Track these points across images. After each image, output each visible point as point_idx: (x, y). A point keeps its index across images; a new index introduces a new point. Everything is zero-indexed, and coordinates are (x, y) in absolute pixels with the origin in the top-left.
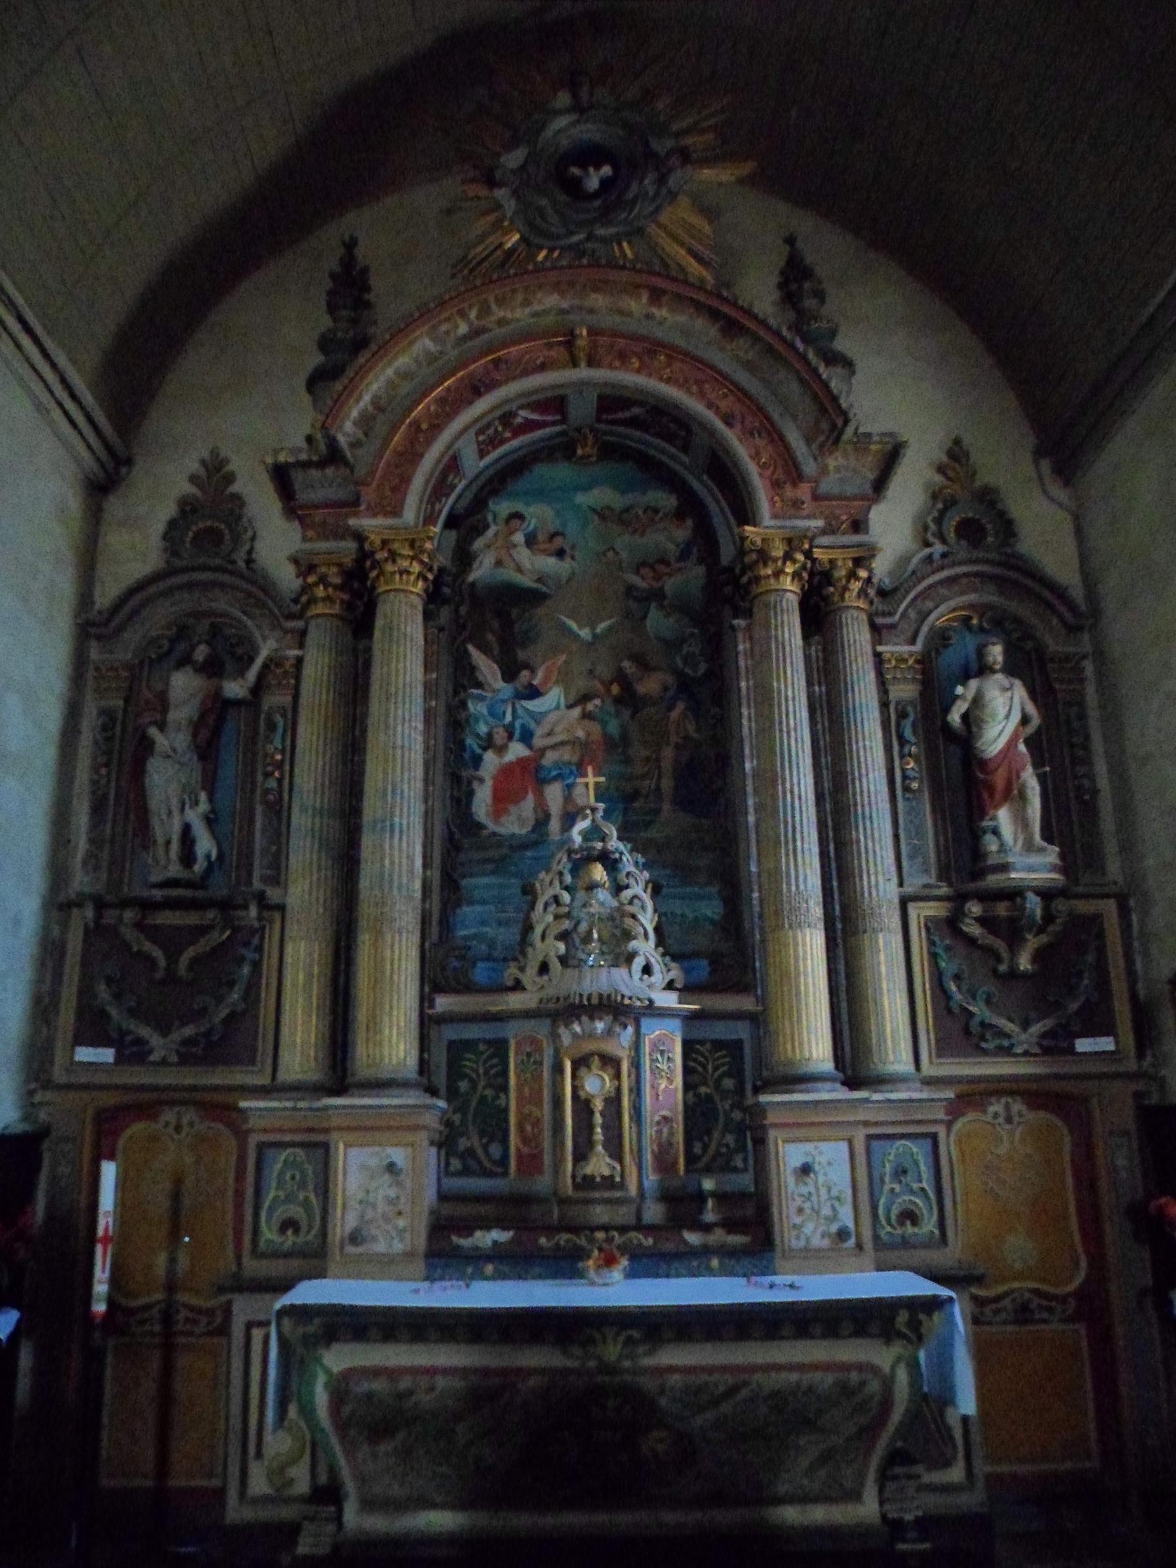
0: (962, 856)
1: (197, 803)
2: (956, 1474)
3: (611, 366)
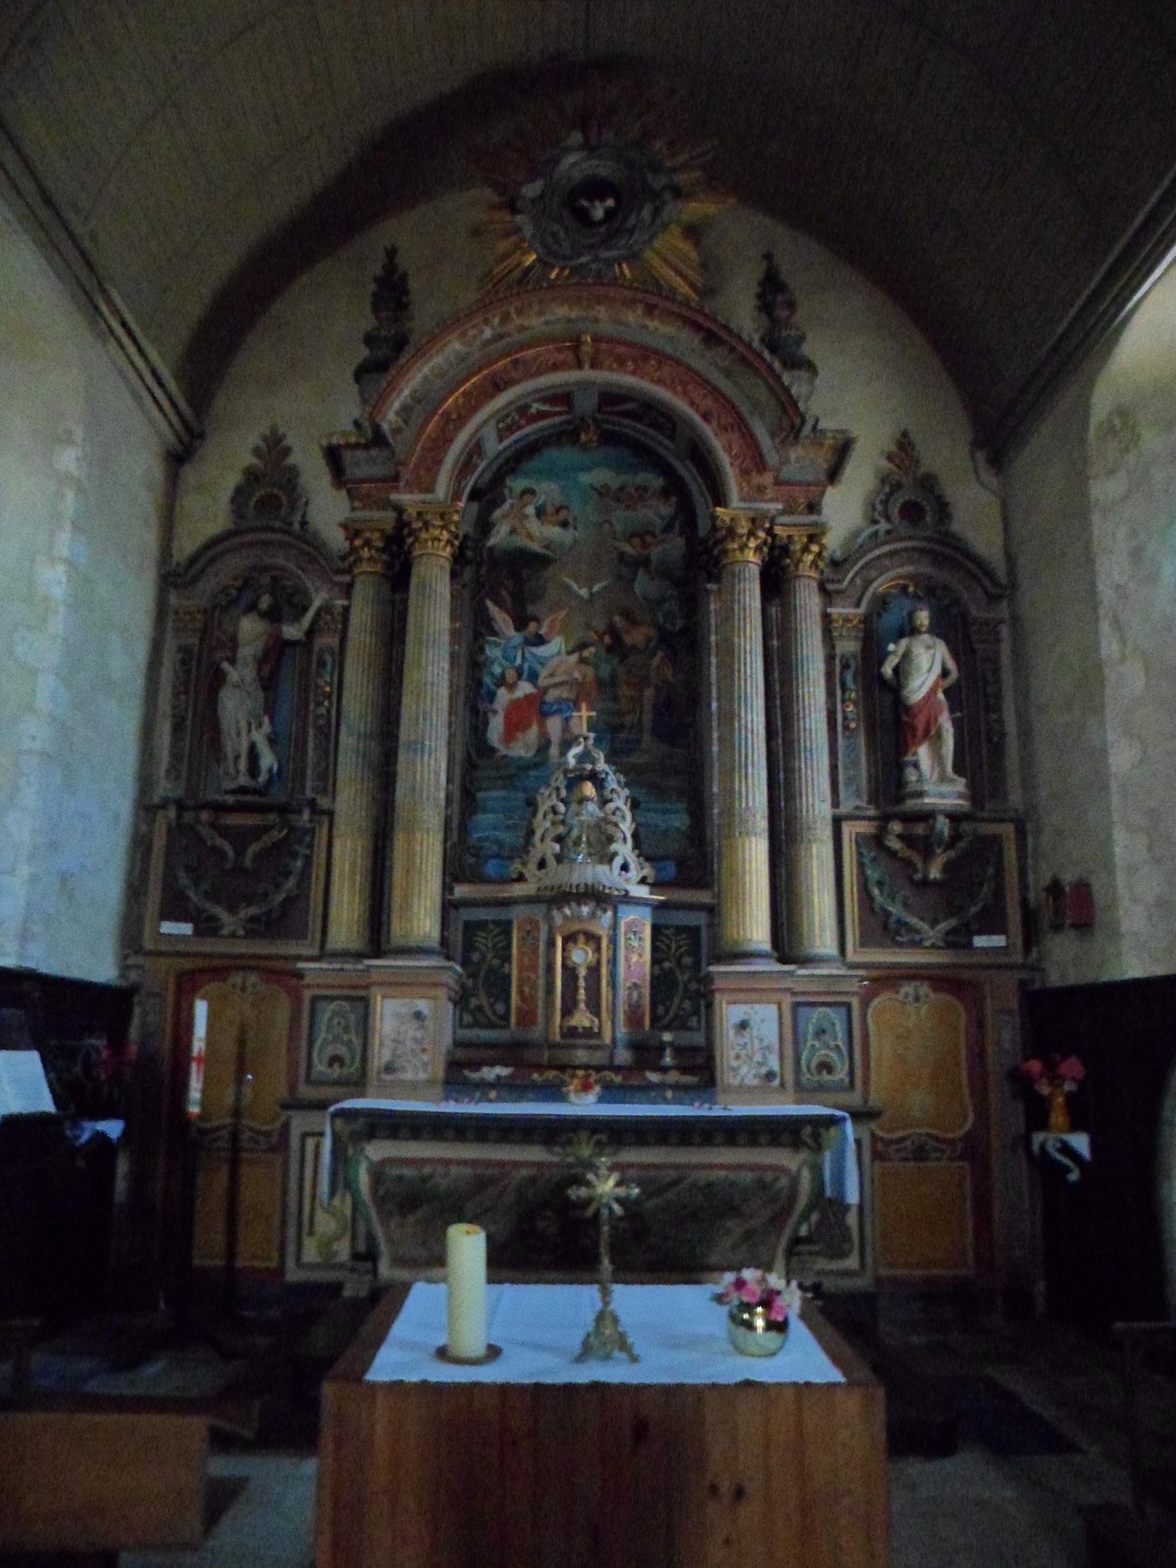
0: (889, 785)
1: (260, 725)
2: (852, 1262)
3: (611, 369)
